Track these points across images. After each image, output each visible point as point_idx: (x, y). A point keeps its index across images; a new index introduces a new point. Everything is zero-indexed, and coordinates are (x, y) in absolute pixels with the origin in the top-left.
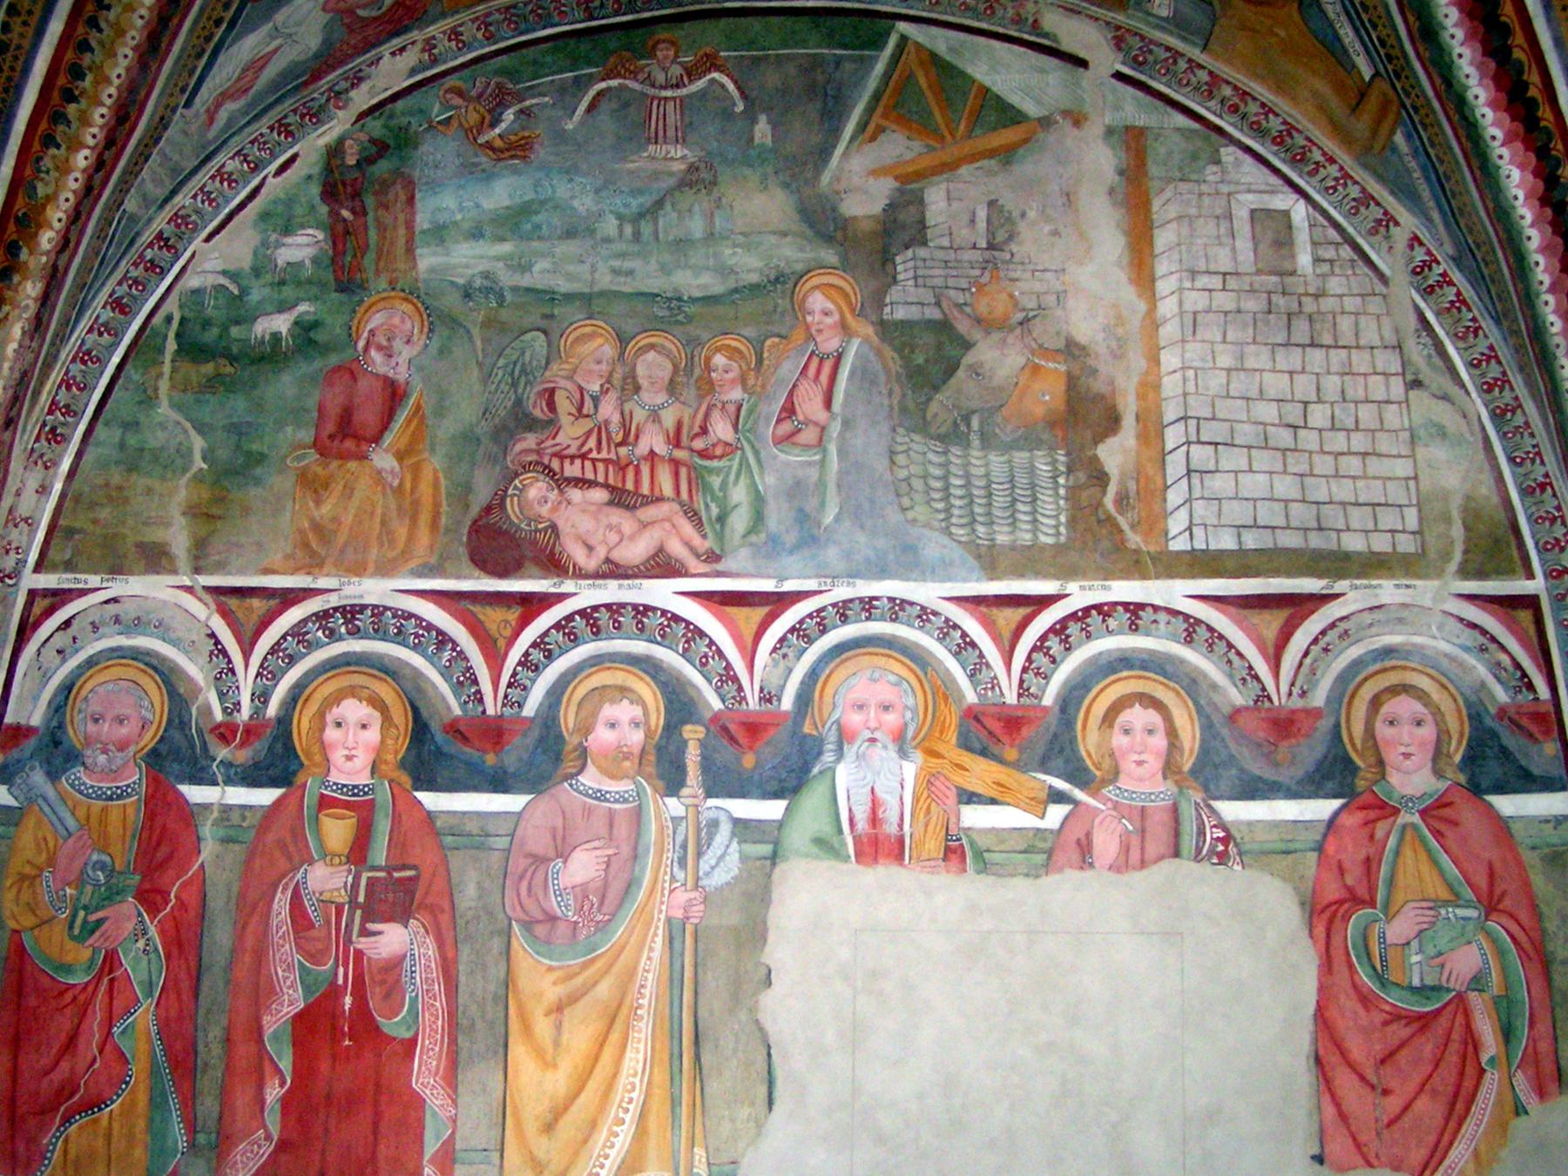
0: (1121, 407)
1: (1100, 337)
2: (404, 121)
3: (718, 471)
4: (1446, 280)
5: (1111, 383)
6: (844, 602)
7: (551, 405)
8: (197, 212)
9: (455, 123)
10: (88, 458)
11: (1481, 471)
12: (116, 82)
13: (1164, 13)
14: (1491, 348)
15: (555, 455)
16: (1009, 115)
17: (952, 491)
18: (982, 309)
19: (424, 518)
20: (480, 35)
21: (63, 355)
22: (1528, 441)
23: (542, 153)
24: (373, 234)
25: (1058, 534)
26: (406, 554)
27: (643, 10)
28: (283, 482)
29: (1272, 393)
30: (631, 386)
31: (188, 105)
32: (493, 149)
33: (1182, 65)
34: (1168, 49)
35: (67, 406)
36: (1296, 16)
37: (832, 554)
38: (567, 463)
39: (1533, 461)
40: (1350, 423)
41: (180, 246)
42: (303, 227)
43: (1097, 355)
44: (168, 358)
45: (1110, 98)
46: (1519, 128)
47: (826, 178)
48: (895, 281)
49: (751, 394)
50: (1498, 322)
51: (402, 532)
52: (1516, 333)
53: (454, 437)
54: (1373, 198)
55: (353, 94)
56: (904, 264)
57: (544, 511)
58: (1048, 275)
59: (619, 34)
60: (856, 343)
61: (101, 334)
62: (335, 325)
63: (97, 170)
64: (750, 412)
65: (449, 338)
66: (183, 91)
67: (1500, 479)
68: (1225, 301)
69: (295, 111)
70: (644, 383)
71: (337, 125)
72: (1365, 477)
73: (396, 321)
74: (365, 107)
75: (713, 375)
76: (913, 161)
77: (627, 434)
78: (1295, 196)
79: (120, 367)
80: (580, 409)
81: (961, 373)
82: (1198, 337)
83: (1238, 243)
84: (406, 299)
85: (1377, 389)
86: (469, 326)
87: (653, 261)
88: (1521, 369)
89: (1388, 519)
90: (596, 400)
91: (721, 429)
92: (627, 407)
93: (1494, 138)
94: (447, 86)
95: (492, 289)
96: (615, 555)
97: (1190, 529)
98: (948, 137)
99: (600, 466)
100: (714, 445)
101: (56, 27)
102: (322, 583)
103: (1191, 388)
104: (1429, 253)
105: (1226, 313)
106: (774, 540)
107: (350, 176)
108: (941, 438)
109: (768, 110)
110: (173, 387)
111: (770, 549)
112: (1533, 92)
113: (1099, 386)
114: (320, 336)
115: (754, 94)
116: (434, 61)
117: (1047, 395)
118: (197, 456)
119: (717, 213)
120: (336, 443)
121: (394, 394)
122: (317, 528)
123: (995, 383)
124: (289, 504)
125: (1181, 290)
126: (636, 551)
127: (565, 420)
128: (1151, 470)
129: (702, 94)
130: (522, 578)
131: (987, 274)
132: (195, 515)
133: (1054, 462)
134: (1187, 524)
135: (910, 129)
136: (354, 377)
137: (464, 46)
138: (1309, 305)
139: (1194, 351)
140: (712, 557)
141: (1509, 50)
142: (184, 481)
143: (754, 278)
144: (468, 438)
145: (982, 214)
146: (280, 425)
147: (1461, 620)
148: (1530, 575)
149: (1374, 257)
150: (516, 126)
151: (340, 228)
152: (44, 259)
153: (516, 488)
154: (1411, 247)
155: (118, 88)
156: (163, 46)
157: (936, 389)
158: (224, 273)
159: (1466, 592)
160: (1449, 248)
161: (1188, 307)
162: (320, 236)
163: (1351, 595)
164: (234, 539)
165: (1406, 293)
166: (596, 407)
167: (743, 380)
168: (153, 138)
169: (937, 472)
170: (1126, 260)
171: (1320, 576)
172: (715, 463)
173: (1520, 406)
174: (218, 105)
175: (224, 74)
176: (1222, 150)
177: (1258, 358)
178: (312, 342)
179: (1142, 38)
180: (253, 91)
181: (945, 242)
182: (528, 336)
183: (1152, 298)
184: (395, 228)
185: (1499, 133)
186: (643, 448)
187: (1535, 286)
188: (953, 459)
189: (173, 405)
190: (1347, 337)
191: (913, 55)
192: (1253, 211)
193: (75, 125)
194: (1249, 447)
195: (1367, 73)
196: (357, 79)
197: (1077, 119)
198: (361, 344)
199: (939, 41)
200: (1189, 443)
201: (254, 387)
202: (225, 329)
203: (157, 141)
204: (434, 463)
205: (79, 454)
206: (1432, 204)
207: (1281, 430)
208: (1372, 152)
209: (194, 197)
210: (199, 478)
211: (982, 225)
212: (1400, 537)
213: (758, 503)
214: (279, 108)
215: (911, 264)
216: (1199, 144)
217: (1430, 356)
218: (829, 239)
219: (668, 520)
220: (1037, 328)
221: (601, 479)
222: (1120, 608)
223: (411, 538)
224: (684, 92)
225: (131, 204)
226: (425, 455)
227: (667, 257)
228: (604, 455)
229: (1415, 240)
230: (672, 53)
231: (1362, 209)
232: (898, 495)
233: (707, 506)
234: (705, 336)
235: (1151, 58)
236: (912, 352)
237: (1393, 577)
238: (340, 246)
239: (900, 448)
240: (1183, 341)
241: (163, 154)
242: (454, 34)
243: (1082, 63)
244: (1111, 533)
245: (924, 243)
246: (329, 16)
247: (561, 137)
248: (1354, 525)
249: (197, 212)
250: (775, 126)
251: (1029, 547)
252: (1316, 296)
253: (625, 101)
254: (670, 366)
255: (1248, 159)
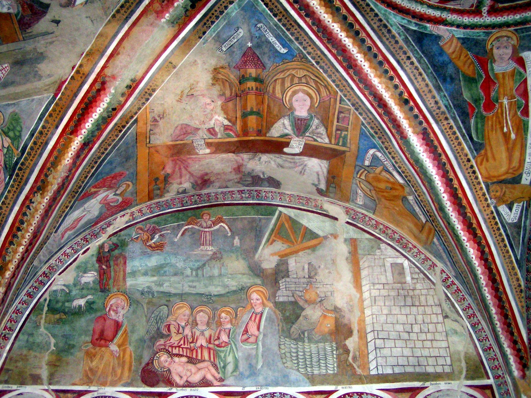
0: (352, 328)
1: (345, 305)
2: (124, 237)
3: (223, 351)
4: (453, 283)
5: (349, 320)
6: (265, 394)
7: (169, 330)
8: (56, 265)
9: (140, 239)
10: (16, 345)
11: (469, 344)
12: (34, 225)
13: (361, 203)
14: (469, 304)
15: (170, 346)
16: (314, 236)
17: (299, 357)
18: (307, 297)
19: (127, 367)
20: (148, 211)
21: (10, 311)
22: (484, 334)
23: (167, 248)
24: (112, 274)
25: (334, 370)
26: (120, 379)
27: (199, 204)
28: (80, 355)
29: (401, 322)
30: (195, 324)
31: (56, 232)
32: (152, 247)
33: (367, 219)
34: (363, 214)
35: (10, 328)
36: (401, 203)
37: (261, 379)
38: (174, 349)
39: (486, 340)
40: (426, 330)
41: (50, 276)
42: (90, 271)
43: (344, 312)
44: (44, 313)
45: (345, 230)
46: (471, 236)
47: (257, 256)
48: (279, 289)
49: (234, 326)
50: (470, 295)
51: (119, 371)
52: (476, 299)
53: (136, 340)
54: (428, 258)
55: (108, 229)
56: (282, 284)
57: (166, 364)
58: (328, 286)
59: (192, 211)
60: (267, 309)
61: (23, 304)
62: (99, 303)
63: (26, 253)
64: (234, 332)
65: (137, 308)
66: (54, 228)
67: (476, 346)
68: (384, 292)
69: (89, 234)
70: (199, 322)
71: (103, 239)
72: (433, 348)
73: (119, 302)
74: (111, 233)
75: (221, 320)
76: (284, 251)
77: (193, 339)
78: (404, 259)
79: (29, 315)
80: (178, 331)
81: (301, 318)
82: (376, 304)
83: (387, 274)
84: (122, 295)
85: (434, 319)
86: (143, 304)
87: (202, 283)
88: (479, 311)
89: (441, 361)
90: (183, 328)
91: (224, 338)
92: (194, 330)
93: (464, 240)
94: (137, 227)
95: (150, 292)
96: (189, 379)
97: (377, 367)
98: (295, 243)
99: (185, 350)
100: (222, 343)
101: (16, 208)
102: (92, 388)
103: (375, 321)
104: (447, 275)
105: (385, 296)
106: (241, 374)
107: (107, 254)
108: (295, 339)
109: (238, 235)
110: (45, 322)
111: (241, 377)
112: (474, 226)
113: (346, 321)
114: (94, 306)
115: (234, 230)
116: (134, 219)
117: (329, 325)
118: (52, 345)
119: (222, 267)
120: (98, 342)
121: (118, 326)
122: (91, 369)
123: (312, 321)
124: (82, 362)
125: (370, 289)
126: (196, 378)
127: (173, 335)
128: (363, 348)
129: (218, 230)
130: (158, 387)
131: (308, 286)
132: (50, 365)
133: (332, 347)
134: (376, 365)
135: (283, 240)
136: (105, 320)
137: (143, 215)
138: (411, 293)
139: (375, 309)
140: (221, 380)
141: (466, 213)
142: (47, 353)
143: (234, 288)
144: (142, 340)
145: (306, 267)
146: (80, 335)
147: (467, 394)
148: (489, 378)
149: (430, 277)
150: (159, 240)
151: (102, 271)
152: (6, 280)
153: (157, 357)
154: (442, 273)
155: (34, 227)
156: (50, 214)
157: (293, 323)
158: (64, 285)
159: (468, 384)
160: (453, 273)
161: (373, 295)
162: (96, 274)
163: (431, 387)
164: (63, 373)
165: (440, 288)
166: (183, 331)
167: (231, 321)
168: (44, 242)
169: (294, 350)
170: (352, 281)
171: (420, 381)
172: (222, 349)
173: (480, 322)
174: (65, 232)
175: (68, 223)
176: (381, 245)
177: (396, 310)
178: (92, 308)
179: (355, 211)
180: (76, 228)
181: (295, 276)
182: (162, 307)
183: (361, 293)
184: (120, 271)
185: (465, 238)
186: (198, 344)
187: (481, 285)
188: (299, 346)
189: (45, 328)
190: (423, 303)
191: (283, 217)
192: (391, 264)
193: (20, 238)
194: (395, 339)
195: (424, 221)
196: (109, 225)
197: (335, 236)
198: (108, 309)
199: (292, 213)
200: (375, 339)
201: (73, 322)
202: (64, 303)
203: (46, 243)
204: (130, 349)
205: (13, 344)
206: (447, 260)
207: (405, 333)
208: (427, 244)
209: (56, 261)
210: (52, 353)
211: (306, 270)
212: (445, 367)
213: (236, 361)
214: (84, 233)
215: (284, 283)
216: (373, 243)
217: (450, 308)
218: (258, 276)
219: (207, 368)
220: (325, 303)
221: (185, 354)
222: (355, 394)
223: (122, 373)
224: (212, 229)
225: (36, 263)
226: (128, 346)
227: (206, 282)
228: (186, 346)
229: (443, 271)
230: (208, 217)
231: (426, 262)
232: (282, 359)
233: (219, 363)
234: (219, 307)
235: (357, 217)
236: (285, 311)
237: (444, 380)
238: (102, 277)
239: (282, 343)
240: (372, 306)
241: (47, 247)
242: (140, 211)
243: (336, 219)
244: (351, 369)
245: (288, 277)
246: (101, 205)
247: (173, 243)
248: (430, 363)
249: (56, 265)
250: (241, 240)
251: (325, 375)
252: (413, 290)
253: (194, 233)
254: (207, 317)
255: (389, 248)
